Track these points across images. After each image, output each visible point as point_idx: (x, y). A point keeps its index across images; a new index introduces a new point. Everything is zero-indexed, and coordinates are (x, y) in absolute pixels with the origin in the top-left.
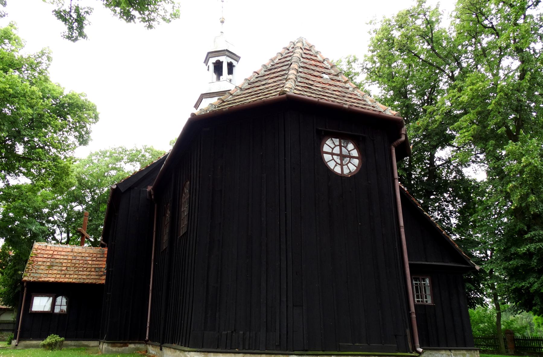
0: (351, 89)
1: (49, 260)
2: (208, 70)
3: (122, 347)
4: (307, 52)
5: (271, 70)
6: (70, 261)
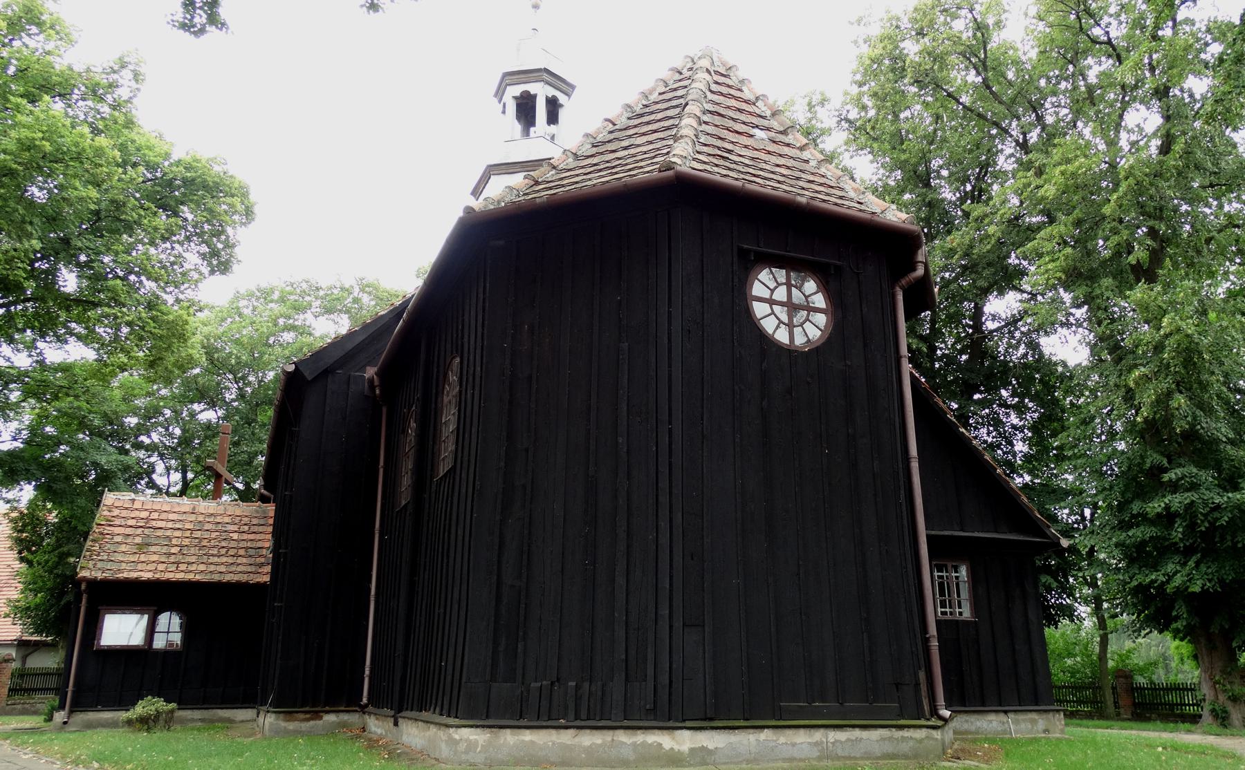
1: (139, 531)
2: (504, 112)
3: (308, 720)
5: (641, 115)
6: (188, 534)
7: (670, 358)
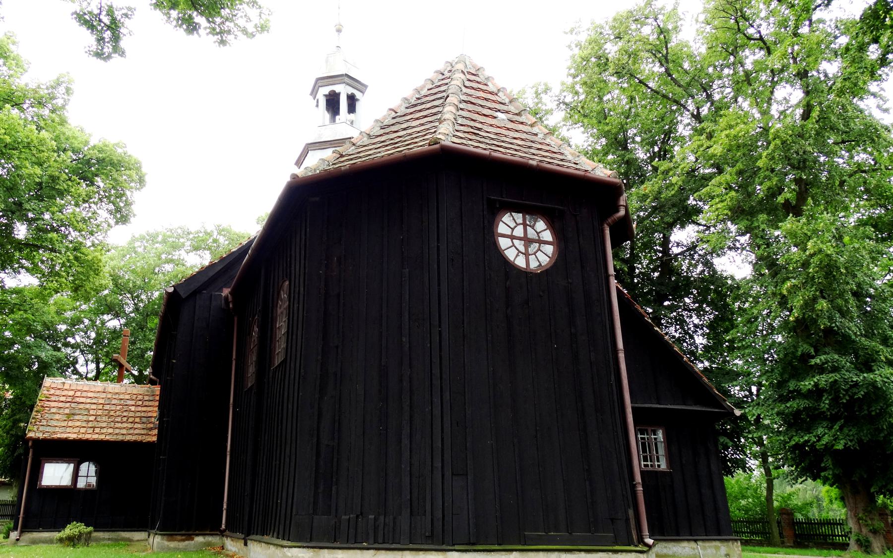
0: (540, 136)
2: (317, 106)
3: (184, 540)
4: (472, 78)
5: (415, 105)
6: (100, 407)
7: (439, 280)
